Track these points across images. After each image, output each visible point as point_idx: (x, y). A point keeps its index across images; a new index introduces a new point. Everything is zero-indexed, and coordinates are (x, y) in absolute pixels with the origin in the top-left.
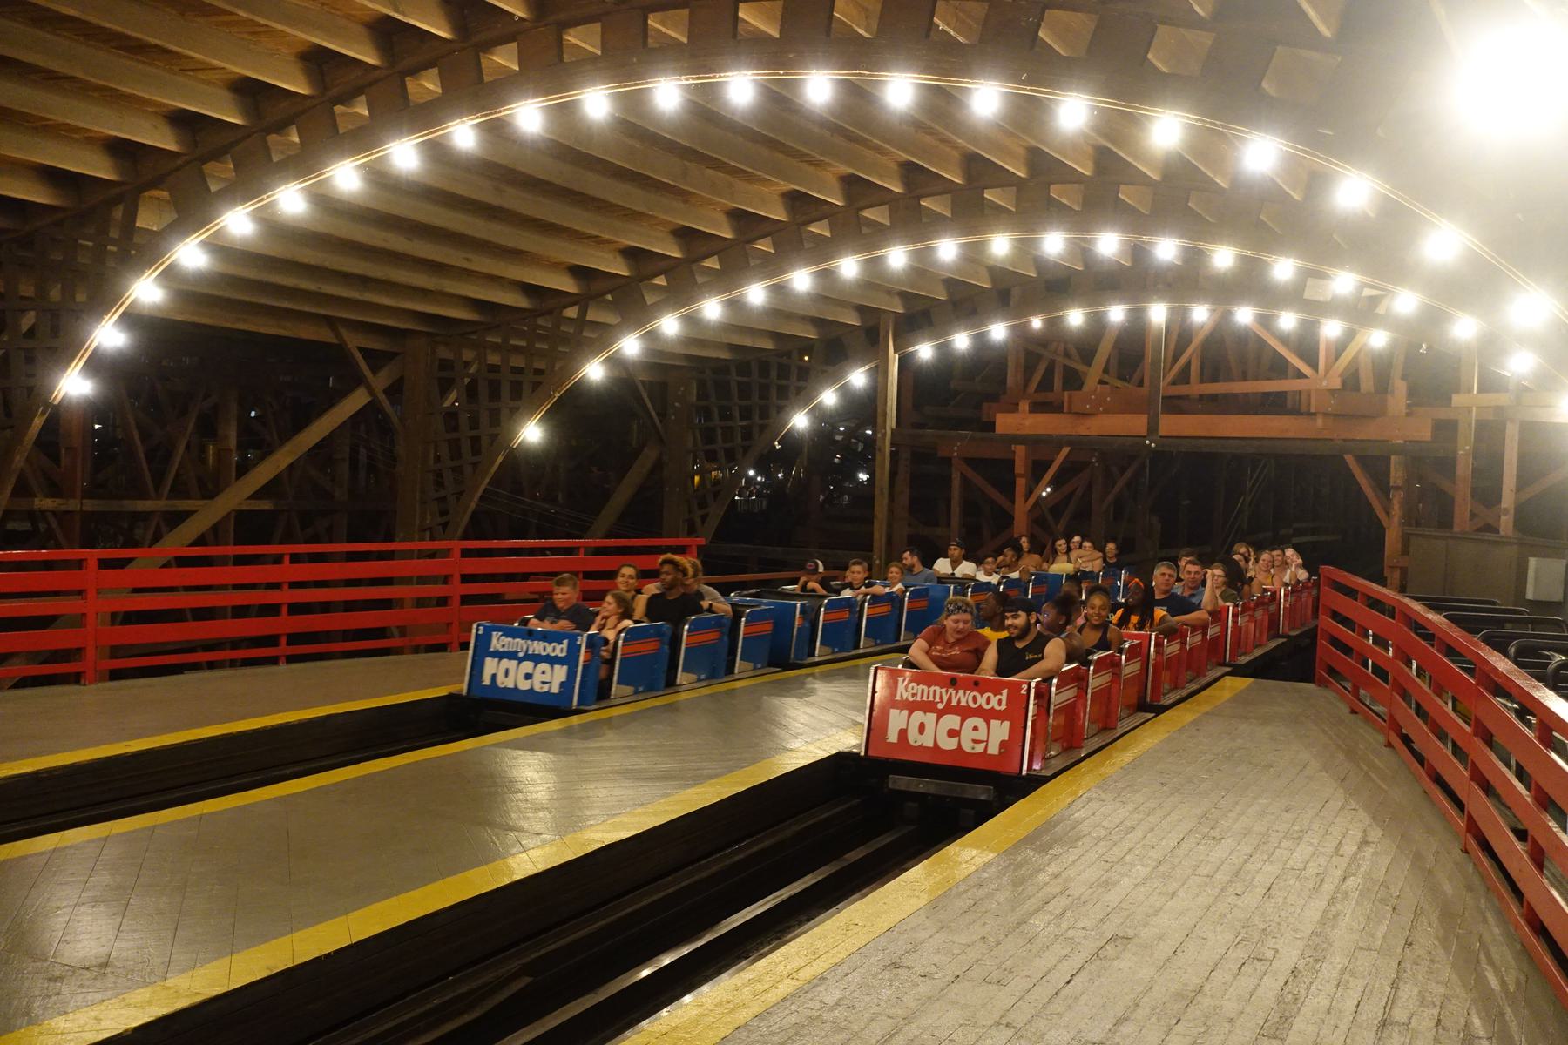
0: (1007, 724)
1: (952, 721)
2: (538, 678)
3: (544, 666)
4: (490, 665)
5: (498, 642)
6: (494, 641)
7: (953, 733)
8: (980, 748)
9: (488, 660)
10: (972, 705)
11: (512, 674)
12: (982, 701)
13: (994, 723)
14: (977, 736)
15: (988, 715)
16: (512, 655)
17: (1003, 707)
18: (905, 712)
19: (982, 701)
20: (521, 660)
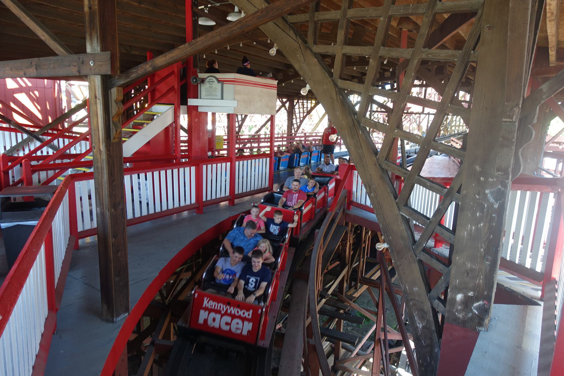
6: (205, 302)
8: (239, 332)
12: (241, 313)
13: (246, 323)
15: (244, 319)
17: (250, 317)
19: (241, 313)
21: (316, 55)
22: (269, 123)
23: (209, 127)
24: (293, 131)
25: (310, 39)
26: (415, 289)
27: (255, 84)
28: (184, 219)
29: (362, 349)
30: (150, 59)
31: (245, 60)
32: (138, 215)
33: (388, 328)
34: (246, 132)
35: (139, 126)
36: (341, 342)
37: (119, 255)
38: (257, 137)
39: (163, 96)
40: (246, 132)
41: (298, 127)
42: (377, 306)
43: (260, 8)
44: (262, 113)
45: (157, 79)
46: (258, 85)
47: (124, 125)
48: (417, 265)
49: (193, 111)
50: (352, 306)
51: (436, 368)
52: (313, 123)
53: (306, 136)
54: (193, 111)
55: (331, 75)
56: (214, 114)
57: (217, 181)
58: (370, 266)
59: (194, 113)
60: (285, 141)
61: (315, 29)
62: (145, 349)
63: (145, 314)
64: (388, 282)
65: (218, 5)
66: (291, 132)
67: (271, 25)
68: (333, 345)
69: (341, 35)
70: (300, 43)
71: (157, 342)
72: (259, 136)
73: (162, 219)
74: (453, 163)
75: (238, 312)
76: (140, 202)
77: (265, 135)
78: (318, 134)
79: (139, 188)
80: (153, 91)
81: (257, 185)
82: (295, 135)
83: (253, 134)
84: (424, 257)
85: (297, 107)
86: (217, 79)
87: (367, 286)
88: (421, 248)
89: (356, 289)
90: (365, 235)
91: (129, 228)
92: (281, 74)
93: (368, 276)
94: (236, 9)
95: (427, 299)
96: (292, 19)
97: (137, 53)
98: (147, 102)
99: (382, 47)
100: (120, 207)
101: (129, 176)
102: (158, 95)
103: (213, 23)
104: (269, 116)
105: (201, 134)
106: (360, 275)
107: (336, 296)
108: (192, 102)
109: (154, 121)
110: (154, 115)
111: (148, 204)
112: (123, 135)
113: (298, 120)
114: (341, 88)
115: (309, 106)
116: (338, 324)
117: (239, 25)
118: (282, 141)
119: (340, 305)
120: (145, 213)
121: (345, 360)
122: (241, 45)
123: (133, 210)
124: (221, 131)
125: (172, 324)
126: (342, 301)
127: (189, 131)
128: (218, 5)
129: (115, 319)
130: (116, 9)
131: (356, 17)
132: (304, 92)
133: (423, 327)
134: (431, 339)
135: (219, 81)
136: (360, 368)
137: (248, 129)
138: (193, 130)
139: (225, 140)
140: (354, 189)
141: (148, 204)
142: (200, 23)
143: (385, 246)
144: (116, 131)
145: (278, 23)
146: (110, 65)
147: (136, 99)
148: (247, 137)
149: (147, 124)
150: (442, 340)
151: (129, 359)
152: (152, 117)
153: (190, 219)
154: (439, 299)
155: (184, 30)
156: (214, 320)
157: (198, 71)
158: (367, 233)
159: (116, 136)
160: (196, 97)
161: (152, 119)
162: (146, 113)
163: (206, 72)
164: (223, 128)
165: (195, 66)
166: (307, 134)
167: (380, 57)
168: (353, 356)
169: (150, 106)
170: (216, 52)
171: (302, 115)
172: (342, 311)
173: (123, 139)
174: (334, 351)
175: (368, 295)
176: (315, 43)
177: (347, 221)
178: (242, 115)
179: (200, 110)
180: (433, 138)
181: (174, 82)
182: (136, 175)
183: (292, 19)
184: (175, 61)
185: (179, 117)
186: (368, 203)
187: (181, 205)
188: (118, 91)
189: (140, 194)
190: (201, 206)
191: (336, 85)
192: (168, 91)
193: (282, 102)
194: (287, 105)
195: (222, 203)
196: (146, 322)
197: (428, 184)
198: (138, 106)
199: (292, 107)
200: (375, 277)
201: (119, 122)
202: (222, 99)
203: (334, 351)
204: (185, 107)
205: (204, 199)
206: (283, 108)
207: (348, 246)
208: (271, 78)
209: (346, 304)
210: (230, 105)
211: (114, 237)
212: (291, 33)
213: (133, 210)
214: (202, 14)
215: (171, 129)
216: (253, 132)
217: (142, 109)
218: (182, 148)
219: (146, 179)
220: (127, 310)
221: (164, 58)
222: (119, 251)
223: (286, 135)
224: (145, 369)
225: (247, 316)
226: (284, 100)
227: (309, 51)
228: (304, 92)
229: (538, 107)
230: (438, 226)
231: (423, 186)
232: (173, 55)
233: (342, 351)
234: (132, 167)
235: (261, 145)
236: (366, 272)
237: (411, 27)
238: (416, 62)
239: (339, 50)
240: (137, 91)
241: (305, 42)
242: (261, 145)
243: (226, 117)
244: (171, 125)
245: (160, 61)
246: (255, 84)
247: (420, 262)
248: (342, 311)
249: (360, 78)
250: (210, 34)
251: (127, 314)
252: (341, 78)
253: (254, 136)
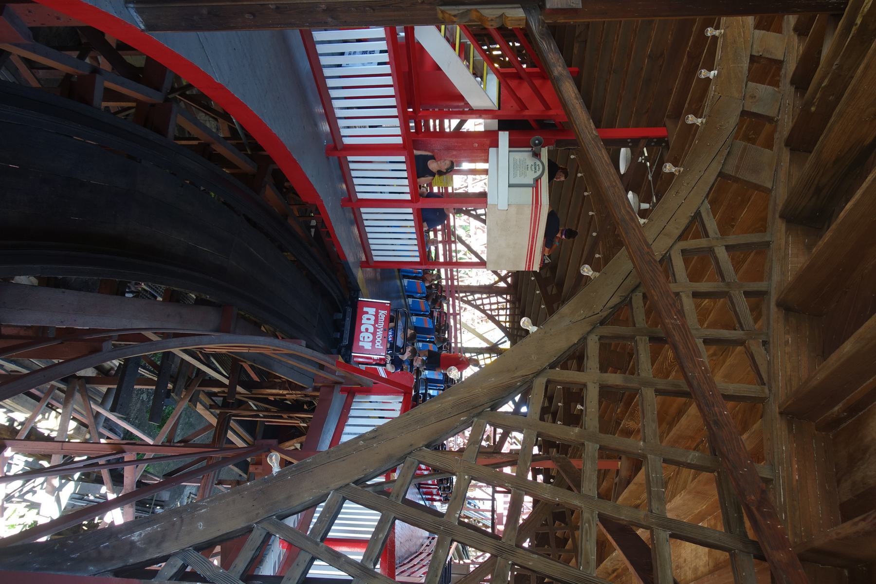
1: (371, 329)
4: (372, 311)
5: (383, 314)
7: (367, 330)
8: (361, 339)
11: (368, 322)
15: (373, 342)
16: (376, 321)
19: (379, 339)
21: (584, 340)
22: (475, 260)
23: (466, 166)
24: (462, 295)
25: (607, 330)
26: (201, 525)
27: (533, 238)
28: (316, 125)
29: (107, 420)
30: (571, 73)
31: (571, 234)
32: (320, 49)
33: (143, 466)
34: (459, 222)
35: (464, 53)
36: (115, 386)
37: (247, 16)
38: (453, 239)
39: (512, 93)
40: (459, 222)
41: (468, 302)
42: (185, 442)
43: (653, 247)
44: (489, 245)
45: (537, 82)
46: (533, 241)
47: (466, 28)
48: (243, 525)
49: (489, 139)
50: (181, 403)
51: (59, 570)
52: (476, 324)
53: (455, 315)
54: (489, 139)
55: (552, 366)
56: (486, 172)
57: (382, 179)
58: (250, 427)
59: (487, 141)
60: (447, 282)
61: (624, 338)
62: (92, 58)
63: (148, 59)
64: (226, 461)
65: (650, 178)
66: (462, 292)
67: (628, 266)
68: (113, 372)
69: (614, 379)
70: (601, 314)
71: (98, 78)
72: (455, 242)
73: (312, 89)
74: (419, 543)
76: (342, 54)
77: (456, 251)
78: (458, 332)
79: (365, 53)
80: (518, 76)
81: (374, 244)
82: (457, 298)
83: (457, 232)
84: (256, 537)
85: (500, 299)
86: (540, 177)
87: (215, 425)
88: (272, 529)
89: (209, 408)
90: (300, 418)
91: (297, 32)
92: (548, 275)
93: (232, 424)
94: (645, 206)
95: (183, 547)
96: (637, 300)
97: (575, 51)
98: (501, 66)
99: (598, 446)
100: (330, 20)
101: (384, 36)
102: (513, 83)
103: (622, 170)
104: (484, 257)
105: (455, 153)
106: (234, 412)
107: (197, 375)
108: (504, 137)
109: (472, 77)
110: (482, 78)
111: (340, 66)
112: (450, 27)
113: (479, 302)
114: (532, 382)
115: (502, 319)
116: (149, 382)
117: (627, 218)
118: (447, 279)
119: (182, 382)
120: (324, 61)
121: (88, 397)
122: (591, 213)
123: (330, 42)
124: (460, 183)
125: (134, 104)
126: (189, 386)
127: (457, 133)
128: (650, 178)
129: (132, 5)
130: (640, 20)
131: (642, 403)
132: (525, 322)
133: (132, 543)
134: (112, 558)
135: (537, 180)
136: (74, 419)
137: (464, 224)
138: (460, 140)
139: (446, 189)
140: (373, 398)
141: (340, 66)
142: (623, 150)
143: (276, 469)
144: (455, 16)
145: (629, 278)
146: (560, 7)
147: (505, 47)
148: (452, 224)
149: (468, 67)
150: (111, 577)
151: (73, 29)
152: (479, 74)
153: (317, 135)
154: (184, 566)
155: (611, 125)
157: (551, 147)
158: (303, 420)
159: (447, 16)
160: (512, 144)
161: (475, 75)
162: (485, 64)
163: (549, 160)
164: (465, 185)
165: (558, 143)
166: (458, 317)
167: (583, 444)
168: (93, 406)
169: (497, 72)
170: (579, 175)
171: (487, 307)
172: (170, 386)
173: (443, 27)
174: (104, 375)
175: (202, 426)
176: (601, 338)
177: (322, 389)
178: (485, 215)
179: (492, 151)
180: (456, 538)
181: (534, 110)
182: (386, 48)
183: (637, 300)
184: (568, 114)
185: (480, 117)
186: (345, 438)
187: (339, 121)
188: (520, 20)
189: (355, 53)
190: (338, 152)
191: (538, 374)
192: (519, 100)
193: (506, 276)
194: (502, 284)
195: (344, 186)
196: (136, 61)
197: (381, 536)
198: (495, 53)
199: (499, 292)
200: (230, 435)
201: (471, 21)
202: (510, 186)
203: (104, 375)
204: (496, 128)
205: (350, 158)
206: (497, 279)
207: (281, 392)
208: (543, 261)
209: (184, 393)
210: (500, 198)
211: (277, 8)
212: (615, 300)
213: (330, 42)
214: (636, 153)
215: (462, 104)
216: (460, 232)
217: (492, 59)
218: (431, 121)
219: (379, 64)
220: (150, 27)
221: (573, 95)
222: (254, 15)
223: (456, 283)
224: (46, 56)
226: (509, 280)
227: (589, 329)
228: (525, 322)
230: (311, 556)
231: (377, 528)
232: (579, 111)
233: (104, 389)
234: (399, 41)
235: (440, 246)
236: (240, 423)
237: (624, 473)
238: (577, 502)
239: (591, 378)
240: (519, 50)
241: (602, 323)
242: (440, 246)
243: (481, 190)
244: (467, 104)
245: (569, 90)
246: (533, 238)
247: (249, 530)
248: (170, 386)
249: (547, 412)
250: (608, 161)
251: (143, 27)
252: (548, 382)
253: (454, 234)
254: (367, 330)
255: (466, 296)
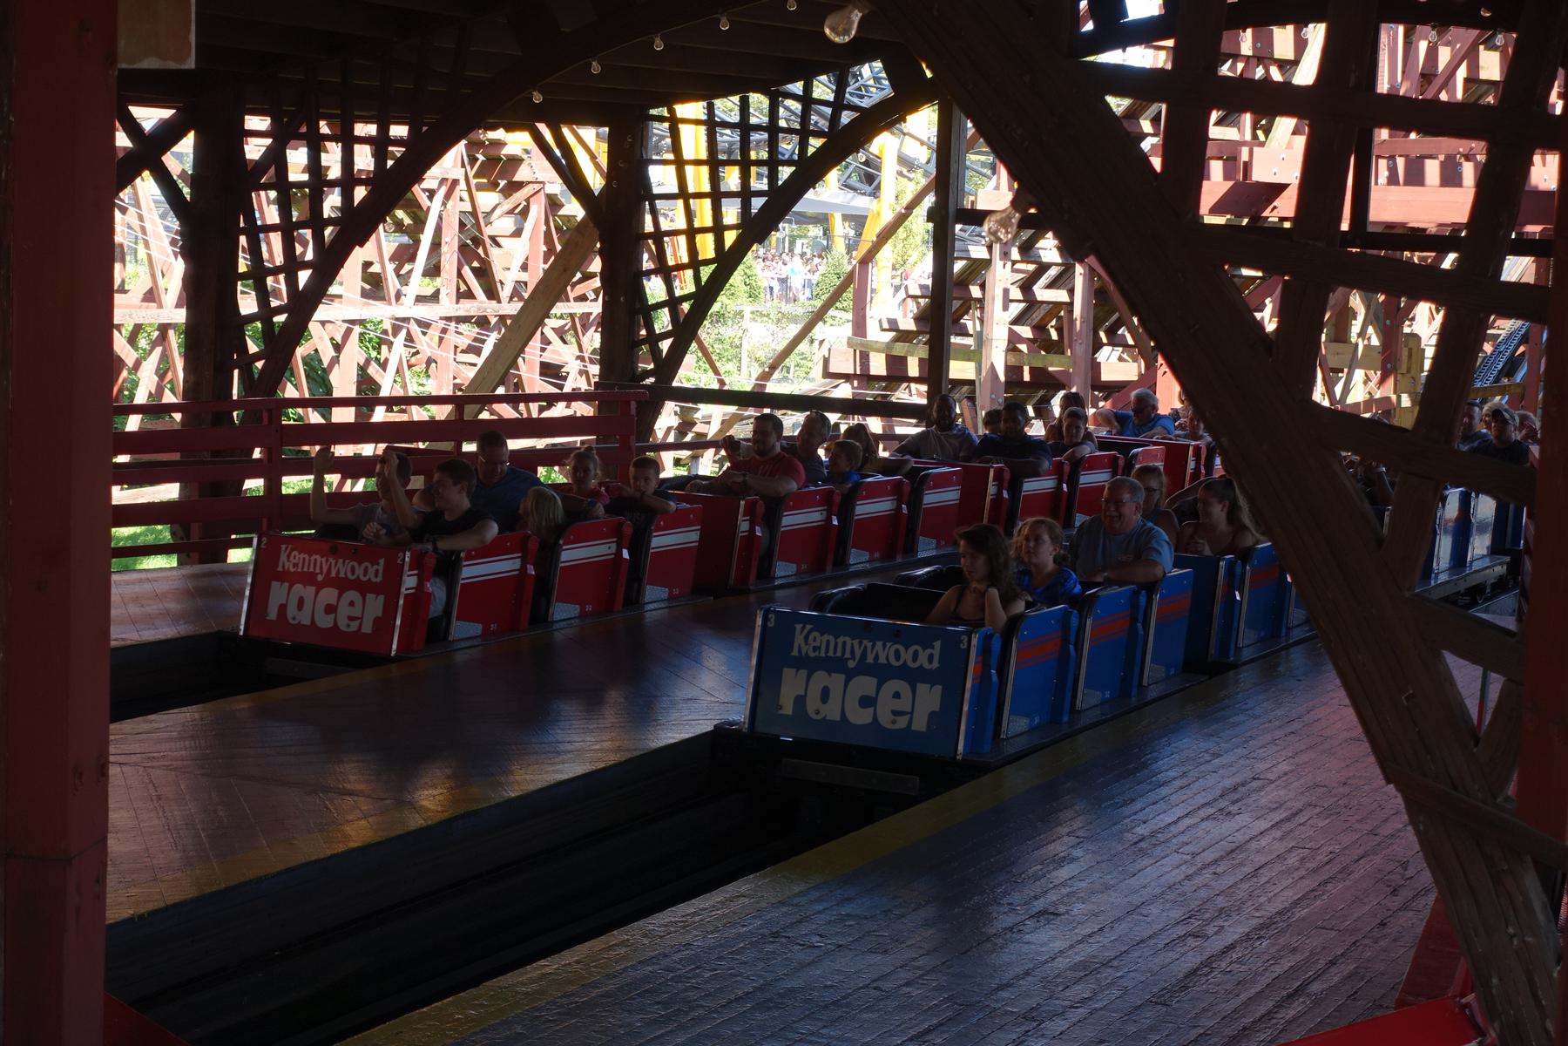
0: (381, 598)
1: (865, 685)
2: (344, 611)
3: (352, 595)
6: (799, 639)
7: (866, 702)
8: (902, 723)
9: (275, 585)
10: (894, 663)
12: (906, 656)
13: (922, 688)
14: (898, 705)
15: (914, 677)
16: (308, 579)
17: (935, 665)
18: (803, 673)
19: (906, 656)
20: (320, 587)
75: (897, 655)
156: (825, 695)
225: (927, 666)
229: (1427, 364)
254: (866, 702)
255: (654, 339)
